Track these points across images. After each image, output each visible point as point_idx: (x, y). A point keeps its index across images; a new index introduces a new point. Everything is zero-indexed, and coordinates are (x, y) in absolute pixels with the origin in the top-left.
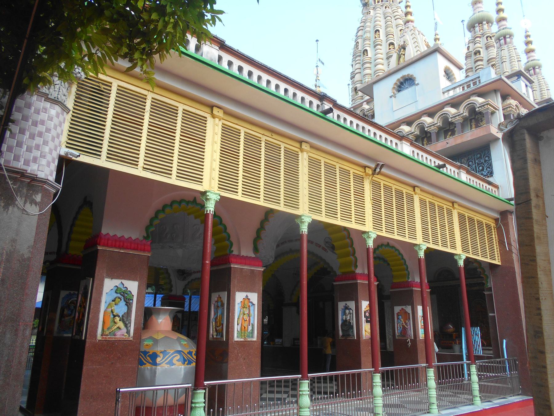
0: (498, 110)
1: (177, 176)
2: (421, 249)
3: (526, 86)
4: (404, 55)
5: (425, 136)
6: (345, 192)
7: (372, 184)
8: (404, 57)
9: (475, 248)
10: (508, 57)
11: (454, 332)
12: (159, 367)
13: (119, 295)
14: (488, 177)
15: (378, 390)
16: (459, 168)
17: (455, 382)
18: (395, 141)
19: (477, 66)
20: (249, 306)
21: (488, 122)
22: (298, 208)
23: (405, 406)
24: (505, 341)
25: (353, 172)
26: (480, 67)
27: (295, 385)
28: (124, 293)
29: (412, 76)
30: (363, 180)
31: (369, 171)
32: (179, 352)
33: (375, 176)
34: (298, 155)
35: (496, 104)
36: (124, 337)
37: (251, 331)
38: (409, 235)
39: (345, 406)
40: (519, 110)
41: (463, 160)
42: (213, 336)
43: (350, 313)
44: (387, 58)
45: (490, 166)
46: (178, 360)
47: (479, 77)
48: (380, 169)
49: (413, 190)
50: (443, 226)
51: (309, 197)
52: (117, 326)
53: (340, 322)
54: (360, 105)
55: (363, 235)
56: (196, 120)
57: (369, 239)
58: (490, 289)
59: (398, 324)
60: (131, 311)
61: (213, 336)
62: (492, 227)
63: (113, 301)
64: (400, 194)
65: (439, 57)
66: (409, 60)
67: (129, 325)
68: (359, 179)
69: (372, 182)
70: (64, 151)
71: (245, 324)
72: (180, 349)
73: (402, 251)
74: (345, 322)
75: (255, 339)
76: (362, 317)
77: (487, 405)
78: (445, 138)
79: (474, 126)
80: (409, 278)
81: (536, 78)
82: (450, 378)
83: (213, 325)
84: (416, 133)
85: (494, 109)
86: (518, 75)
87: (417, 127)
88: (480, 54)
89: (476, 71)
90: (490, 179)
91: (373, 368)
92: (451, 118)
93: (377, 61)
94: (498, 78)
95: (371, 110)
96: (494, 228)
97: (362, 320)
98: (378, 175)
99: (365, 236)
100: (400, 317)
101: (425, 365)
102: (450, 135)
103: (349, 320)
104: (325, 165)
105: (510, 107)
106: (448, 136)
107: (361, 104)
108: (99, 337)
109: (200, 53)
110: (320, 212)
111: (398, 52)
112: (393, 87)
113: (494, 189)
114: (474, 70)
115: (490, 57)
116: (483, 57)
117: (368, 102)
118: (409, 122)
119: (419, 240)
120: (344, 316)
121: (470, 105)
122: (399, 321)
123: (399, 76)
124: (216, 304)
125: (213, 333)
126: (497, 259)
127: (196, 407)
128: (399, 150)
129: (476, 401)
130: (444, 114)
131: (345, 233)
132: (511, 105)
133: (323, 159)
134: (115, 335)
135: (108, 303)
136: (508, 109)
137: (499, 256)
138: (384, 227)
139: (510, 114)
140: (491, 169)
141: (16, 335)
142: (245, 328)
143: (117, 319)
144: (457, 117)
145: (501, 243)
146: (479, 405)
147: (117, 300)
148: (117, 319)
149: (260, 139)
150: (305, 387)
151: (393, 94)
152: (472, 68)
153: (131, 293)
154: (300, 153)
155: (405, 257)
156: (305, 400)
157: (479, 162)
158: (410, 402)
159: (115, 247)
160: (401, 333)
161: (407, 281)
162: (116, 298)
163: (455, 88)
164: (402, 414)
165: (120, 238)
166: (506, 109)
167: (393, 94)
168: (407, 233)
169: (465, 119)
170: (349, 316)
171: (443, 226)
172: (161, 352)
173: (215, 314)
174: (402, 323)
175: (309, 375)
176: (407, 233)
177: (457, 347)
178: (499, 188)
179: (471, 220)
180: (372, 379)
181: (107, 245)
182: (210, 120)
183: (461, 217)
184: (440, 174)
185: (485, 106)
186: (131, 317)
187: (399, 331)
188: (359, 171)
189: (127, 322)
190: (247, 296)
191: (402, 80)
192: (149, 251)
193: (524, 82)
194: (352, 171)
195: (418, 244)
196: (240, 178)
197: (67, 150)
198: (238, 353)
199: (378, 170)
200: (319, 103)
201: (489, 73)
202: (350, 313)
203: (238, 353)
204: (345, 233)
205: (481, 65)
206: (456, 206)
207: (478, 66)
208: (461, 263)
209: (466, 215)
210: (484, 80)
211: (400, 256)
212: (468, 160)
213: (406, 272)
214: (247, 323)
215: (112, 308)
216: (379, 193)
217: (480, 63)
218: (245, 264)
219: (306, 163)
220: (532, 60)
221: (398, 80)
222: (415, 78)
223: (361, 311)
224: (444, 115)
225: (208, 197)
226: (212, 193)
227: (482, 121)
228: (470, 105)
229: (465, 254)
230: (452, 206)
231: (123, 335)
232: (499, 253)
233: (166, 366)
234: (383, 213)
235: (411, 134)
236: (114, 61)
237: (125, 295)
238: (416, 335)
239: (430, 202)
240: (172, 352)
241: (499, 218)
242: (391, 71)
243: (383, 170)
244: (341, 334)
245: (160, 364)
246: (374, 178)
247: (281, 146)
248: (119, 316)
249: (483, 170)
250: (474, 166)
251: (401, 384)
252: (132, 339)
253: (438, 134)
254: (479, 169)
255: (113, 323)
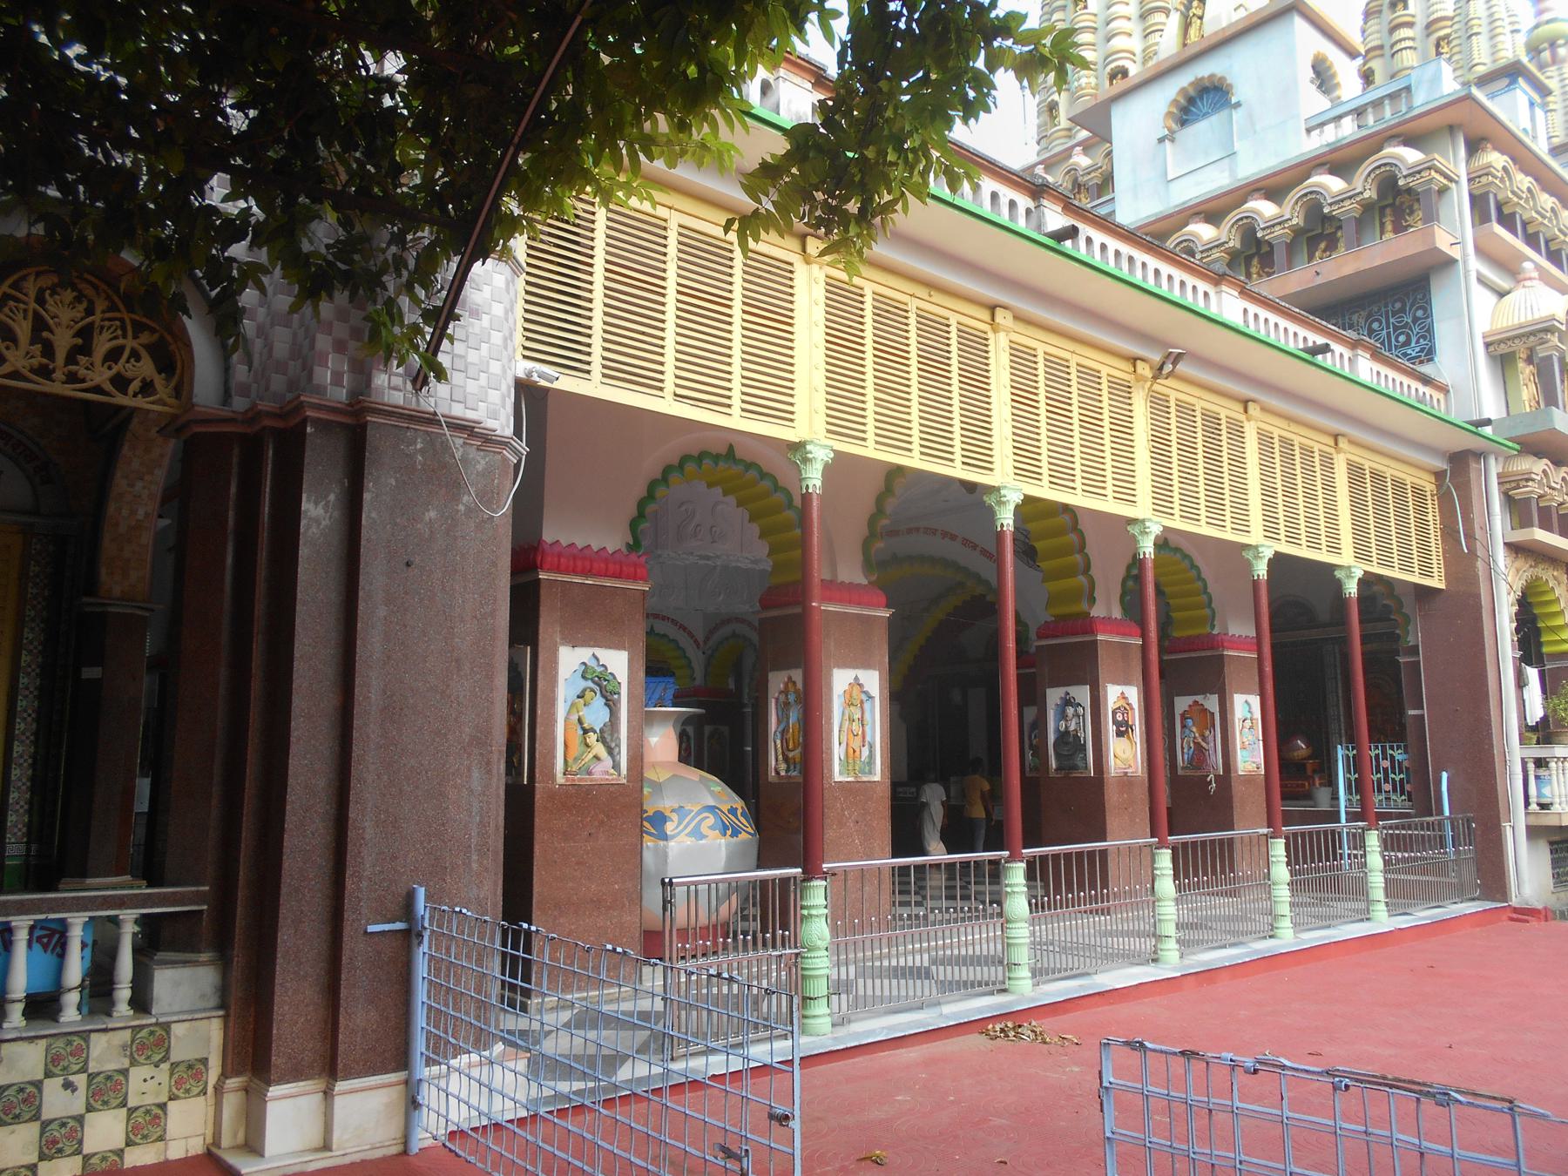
0: (1456, 182)
1: (743, 410)
2: (1004, 503)
3: (1532, 104)
4: (1201, 18)
5: (1254, 250)
6: (1091, 423)
7: (1151, 402)
8: (1201, 24)
9: (1385, 550)
10: (1484, 22)
11: (1309, 757)
12: (672, 844)
13: (590, 684)
14: (1421, 362)
15: (1166, 885)
16: (1354, 345)
17: (1317, 870)
18: (1203, 286)
19: (1396, 43)
20: (862, 702)
21: (1431, 217)
22: (991, 470)
23: (1214, 926)
24: (1445, 775)
25: (1108, 375)
26: (1404, 44)
27: (996, 872)
28: (600, 678)
29: (1222, 79)
30: (1129, 393)
31: (1144, 370)
32: (711, 809)
33: (1158, 381)
34: (986, 339)
35: (1451, 167)
36: (610, 778)
37: (867, 760)
38: (1181, 510)
39: (1074, 927)
40: (1510, 179)
41: (1355, 317)
42: (777, 773)
43: (1076, 715)
44: (1141, 16)
45: (1428, 333)
46: (712, 828)
47: (1408, 89)
48: (1175, 363)
49: (1242, 410)
50: (1310, 496)
51: (828, 393)
52: (594, 752)
53: (1051, 738)
54: (1063, 155)
55: (1129, 528)
56: (769, 272)
57: (1259, 561)
58: (1414, 650)
59: (1183, 740)
60: (618, 719)
61: (777, 773)
62: (1428, 494)
63: (578, 697)
64: (1212, 421)
65: (1298, 23)
66: (1216, 33)
67: (617, 750)
68: (1122, 391)
69: (1152, 396)
70: (522, 370)
71: (856, 743)
72: (712, 803)
73: (1199, 562)
74: (1063, 736)
75: (877, 778)
76: (1107, 723)
77: (1403, 922)
78: (1311, 258)
79: (1389, 227)
80: (1213, 627)
81: (1555, 74)
82: (1320, 860)
83: (776, 746)
84: (1231, 244)
85: (1445, 182)
86: (1511, 72)
87: (1235, 227)
88: (1406, 7)
89: (1393, 55)
90: (1426, 369)
91: (1152, 837)
92: (1331, 205)
93: (1113, 25)
94: (1463, 94)
95: (1097, 169)
96: (1432, 495)
97: (1107, 731)
98: (1166, 378)
99: (1131, 529)
100: (1190, 722)
101: (1265, 831)
102: (1324, 251)
103: (1076, 730)
104: (1046, 360)
105: (1487, 174)
106: (1317, 254)
107: (1068, 153)
108: (560, 779)
109: (771, 100)
110: (1037, 477)
111: (1182, 8)
112: (1166, 110)
113: (1437, 395)
114: (1388, 52)
115: (1435, 16)
116: (1413, 16)
117: (1087, 147)
118: (1212, 211)
119: (1255, 536)
120: (1063, 723)
121: (1383, 169)
122: (1187, 731)
123: (1184, 80)
124: (782, 698)
125: (777, 764)
126: (1436, 574)
127: (811, 916)
128: (1213, 311)
129: (1375, 913)
130: (1311, 193)
131: (1066, 518)
132: (1492, 170)
133: (1042, 345)
134: (590, 773)
135: (569, 703)
136: (1484, 180)
137: (1442, 566)
138: (1176, 505)
139: (1487, 193)
140: (1430, 341)
141: (489, 772)
142: (854, 751)
143: (592, 738)
144: (1347, 203)
145: (1449, 533)
146: (1383, 920)
147: (589, 694)
148: (592, 738)
149: (904, 307)
150: (1017, 875)
151: (1167, 132)
152: (1381, 47)
153: (615, 678)
154: (990, 335)
155: (1206, 573)
156: (1018, 902)
157: (1399, 322)
158: (1217, 919)
159: (575, 572)
160: (1190, 761)
161: (1210, 636)
162: (584, 691)
163: (1340, 117)
164: (1202, 940)
165: (582, 549)
166: (1477, 180)
167: (1167, 132)
168: (1228, 518)
169: (1368, 207)
170: (1073, 723)
171: (1310, 496)
172: (672, 811)
173: (779, 722)
174: (1195, 738)
175: (1024, 851)
176: (1228, 518)
177: (1323, 795)
178: (1448, 391)
179: (1377, 477)
180: (1153, 861)
181: (558, 570)
182: (800, 269)
183: (1355, 472)
184: (1314, 368)
185: (1423, 174)
186: (618, 731)
187: (1186, 756)
188: (1121, 370)
189: (613, 745)
190: (856, 678)
191: (1192, 92)
192: (644, 579)
193: (1526, 93)
194: (1105, 371)
195: (1254, 543)
196: (870, 406)
197: (530, 365)
198: (843, 810)
199: (1168, 368)
200: (1031, 204)
201: (1436, 79)
202: (1076, 715)
203: (843, 810)
204: (1065, 519)
205: (1409, 39)
206: (1343, 443)
207: (1400, 41)
208: (1352, 588)
209: (1366, 467)
210: (1422, 99)
211: (1194, 572)
212: (1369, 315)
213: (1207, 611)
214: (858, 740)
215: (581, 714)
216: (1125, 410)
217: (1404, 32)
218: (850, 602)
219: (1005, 358)
220: (1548, 22)
221: (1183, 91)
222: (1230, 86)
223: (1106, 709)
224: (1309, 197)
225: (810, 456)
226: (816, 445)
227: (1412, 212)
228: (1383, 169)
229: (1362, 565)
230: (1332, 444)
231: (607, 773)
232: (1441, 558)
233: (689, 841)
234: (1043, 431)
235: (1217, 246)
236: (642, 157)
237: (602, 683)
238: (1229, 764)
239: (1282, 439)
240: (696, 810)
241: (1446, 470)
242: (1163, 67)
243: (1181, 367)
244: (1054, 766)
245: (673, 837)
246: (1156, 387)
247: (865, 289)
248: (595, 732)
249: (1407, 343)
250: (1384, 332)
251: (1214, 872)
252: (624, 781)
253: (1291, 248)
254: (1397, 341)
255: (583, 748)
